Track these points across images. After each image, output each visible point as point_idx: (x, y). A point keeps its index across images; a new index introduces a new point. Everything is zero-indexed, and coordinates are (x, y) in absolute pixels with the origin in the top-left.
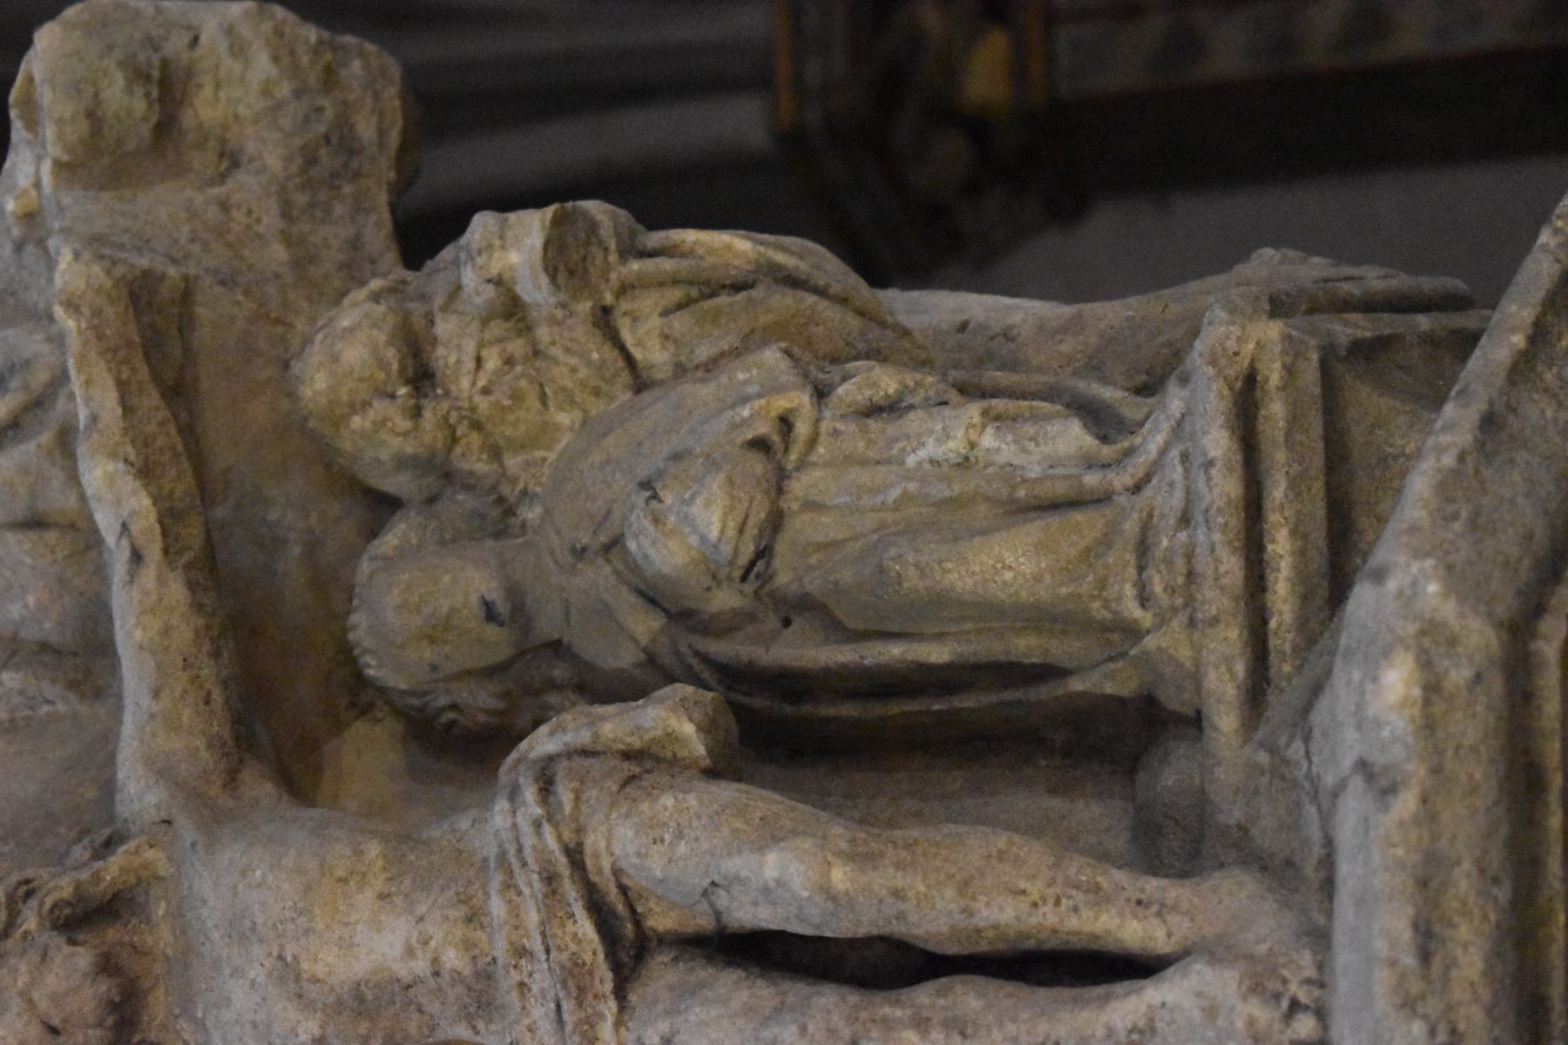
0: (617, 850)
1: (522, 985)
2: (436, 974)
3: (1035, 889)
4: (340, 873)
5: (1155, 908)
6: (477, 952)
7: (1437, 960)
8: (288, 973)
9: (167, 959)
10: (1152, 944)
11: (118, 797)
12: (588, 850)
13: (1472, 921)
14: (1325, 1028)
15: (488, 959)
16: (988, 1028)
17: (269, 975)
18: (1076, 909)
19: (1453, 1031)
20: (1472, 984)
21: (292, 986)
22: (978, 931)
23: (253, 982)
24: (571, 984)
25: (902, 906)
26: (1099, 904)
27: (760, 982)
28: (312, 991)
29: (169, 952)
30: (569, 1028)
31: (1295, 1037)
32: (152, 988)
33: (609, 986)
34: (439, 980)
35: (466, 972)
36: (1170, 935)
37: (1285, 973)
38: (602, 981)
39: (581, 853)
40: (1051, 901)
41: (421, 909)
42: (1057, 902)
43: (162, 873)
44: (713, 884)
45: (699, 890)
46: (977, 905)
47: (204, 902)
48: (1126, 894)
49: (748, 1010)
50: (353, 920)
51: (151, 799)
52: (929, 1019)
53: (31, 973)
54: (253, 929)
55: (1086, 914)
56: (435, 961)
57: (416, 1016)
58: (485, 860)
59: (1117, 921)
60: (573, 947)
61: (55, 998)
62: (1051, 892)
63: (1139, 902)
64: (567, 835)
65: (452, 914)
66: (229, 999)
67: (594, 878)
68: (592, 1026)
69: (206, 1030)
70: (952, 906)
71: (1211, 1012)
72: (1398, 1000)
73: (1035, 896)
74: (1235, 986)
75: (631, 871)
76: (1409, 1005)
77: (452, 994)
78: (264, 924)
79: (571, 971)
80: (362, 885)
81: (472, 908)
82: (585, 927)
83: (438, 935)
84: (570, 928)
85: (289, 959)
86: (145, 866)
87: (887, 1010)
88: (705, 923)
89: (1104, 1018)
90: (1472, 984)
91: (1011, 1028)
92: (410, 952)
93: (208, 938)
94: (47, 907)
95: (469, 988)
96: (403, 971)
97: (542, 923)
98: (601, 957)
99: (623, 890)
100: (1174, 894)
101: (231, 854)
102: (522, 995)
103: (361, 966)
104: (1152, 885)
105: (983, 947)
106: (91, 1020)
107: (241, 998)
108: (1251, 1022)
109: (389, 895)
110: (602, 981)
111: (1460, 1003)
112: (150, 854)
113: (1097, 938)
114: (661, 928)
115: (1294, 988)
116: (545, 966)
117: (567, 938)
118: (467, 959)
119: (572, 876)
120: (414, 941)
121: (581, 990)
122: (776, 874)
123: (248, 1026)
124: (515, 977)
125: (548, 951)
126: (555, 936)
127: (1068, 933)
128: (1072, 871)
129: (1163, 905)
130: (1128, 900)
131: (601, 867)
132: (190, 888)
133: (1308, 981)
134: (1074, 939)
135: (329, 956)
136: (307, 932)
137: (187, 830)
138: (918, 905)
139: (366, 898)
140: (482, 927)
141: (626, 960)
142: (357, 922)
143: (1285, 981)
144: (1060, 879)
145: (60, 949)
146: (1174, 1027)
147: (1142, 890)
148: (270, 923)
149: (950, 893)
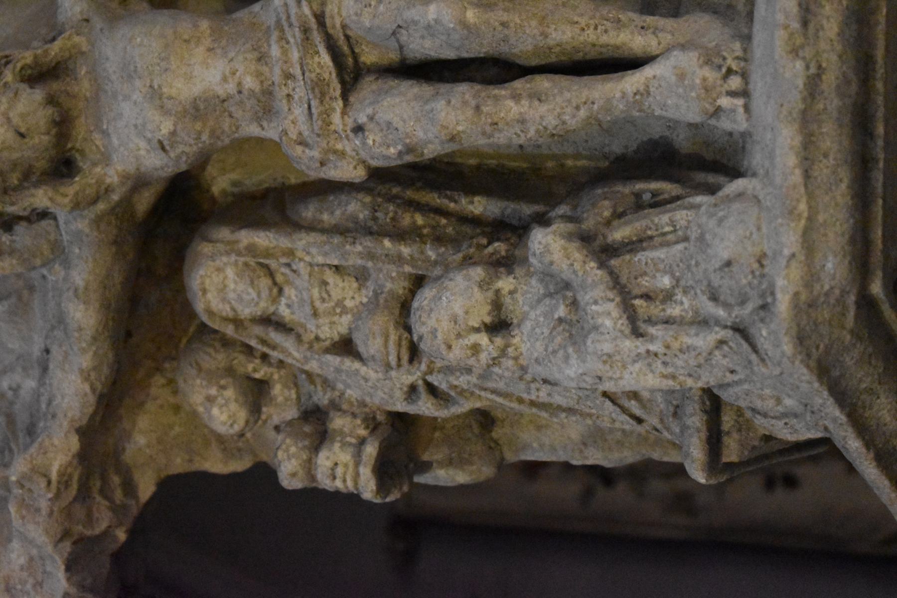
0: (344, 14)
1: (288, 95)
2: (240, 92)
3: (583, 21)
4: (186, 37)
5: (651, 30)
6: (263, 78)
7: (811, 26)
8: (155, 94)
9: (87, 100)
10: (649, 49)
11: (60, 10)
12: (327, 14)
13: (832, 4)
14: (747, 83)
15: (270, 82)
16: (554, 96)
17: (144, 97)
18: (606, 31)
19: (820, 67)
20: (831, 40)
21: (158, 102)
22: (550, 48)
23: (135, 103)
24: (317, 90)
25: (506, 32)
26: (619, 29)
27: (424, 85)
28: (169, 104)
29: (88, 94)
30: (315, 117)
31: (729, 89)
32: (77, 117)
33: (338, 92)
34: (241, 96)
35: (257, 90)
36: (659, 44)
37: (725, 54)
38: (334, 90)
39: (324, 17)
40: (592, 28)
41: (232, 54)
42: (596, 28)
43: (84, 49)
44: (399, 27)
45: (391, 31)
46: (550, 30)
47: (107, 59)
48: (635, 23)
49: (417, 98)
50: (192, 62)
51: (78, 9)
52: (520, 94)
53: (9, 103)
54: (135, 71)
55: (612, 33)
56: (239, 84)
57: (228, 120)
58: (269, 27)
59: (630, 37)
60: (318, 71)
61: (23, 116)
62: (592, 22)
63: (643, 28)
64: (315, 7)
65: (249, 56)
66: (122, 114)
67: (331, 31)
68: (328, 116)
69: (109, 135)
70: (536, 31)
71: (682, 77)
72: (789, 49)
73: (583, 25)
74: (695, 60)
75: (352, 26)
76: (795, 52)
77: (249, 104)
78: (142, 67)
79: (317, 83)
80: (197, 45)
81: (260, 53)
82: (325, 58)
83: (241, 69)
84: (316, 59)
85: (156, 87)
86: (74, 46)
87: (496, 92)
88: (393, 56)
89: (620, 87)
90: (831, 40)
91: (567, 95)
92: (225, 79)
93: (110, 80)
94: (18, 68)
95: (259, 101)
96: (221, 92)
97: (301, 58)
98: (334, 75)
99: (348, 38)
100: (663, 23)
101: (124, 31)
102: (289, 101)
103: (197, 89)
104: (649, 19)
105: (553, 59)
106: (43, 129)
107: (126, 108)
108: (704, 79)
109: (213, 49)
110: (334, 90)
111: (824, 51)
112: (76, 39)
113: (618, 48)
114: (368, 62)
115: (730, 62)
116: (302, 83)
117: (315, 66)
118: (258, 83)
119: (318, 29)
120: (227, 73)
121: (323, 94)
122: (435, 16)
123: (133, 128)
124: (285, 91)
125: (303, 74)
126: (308, 64)
127: (601, 46)
128: (605, 12)
129: (656, 29)
130: (636, 26)
131: (334, 23)
132: (100, 53)
133: (737, 58)
134: (604, 50)
135: (179, 84)
136: (166, 70)
137: (98, 23)
138: (516, 32)
139: (201, 49)
140: (266, 64)
141: (348, 80)
142: (195, 64)
143: (724, 59)
144: (598, 14)
145: (25, 90)
146: (660, 89)
147: (645, 21)
148: (145, 67)
149: (534, 23)
